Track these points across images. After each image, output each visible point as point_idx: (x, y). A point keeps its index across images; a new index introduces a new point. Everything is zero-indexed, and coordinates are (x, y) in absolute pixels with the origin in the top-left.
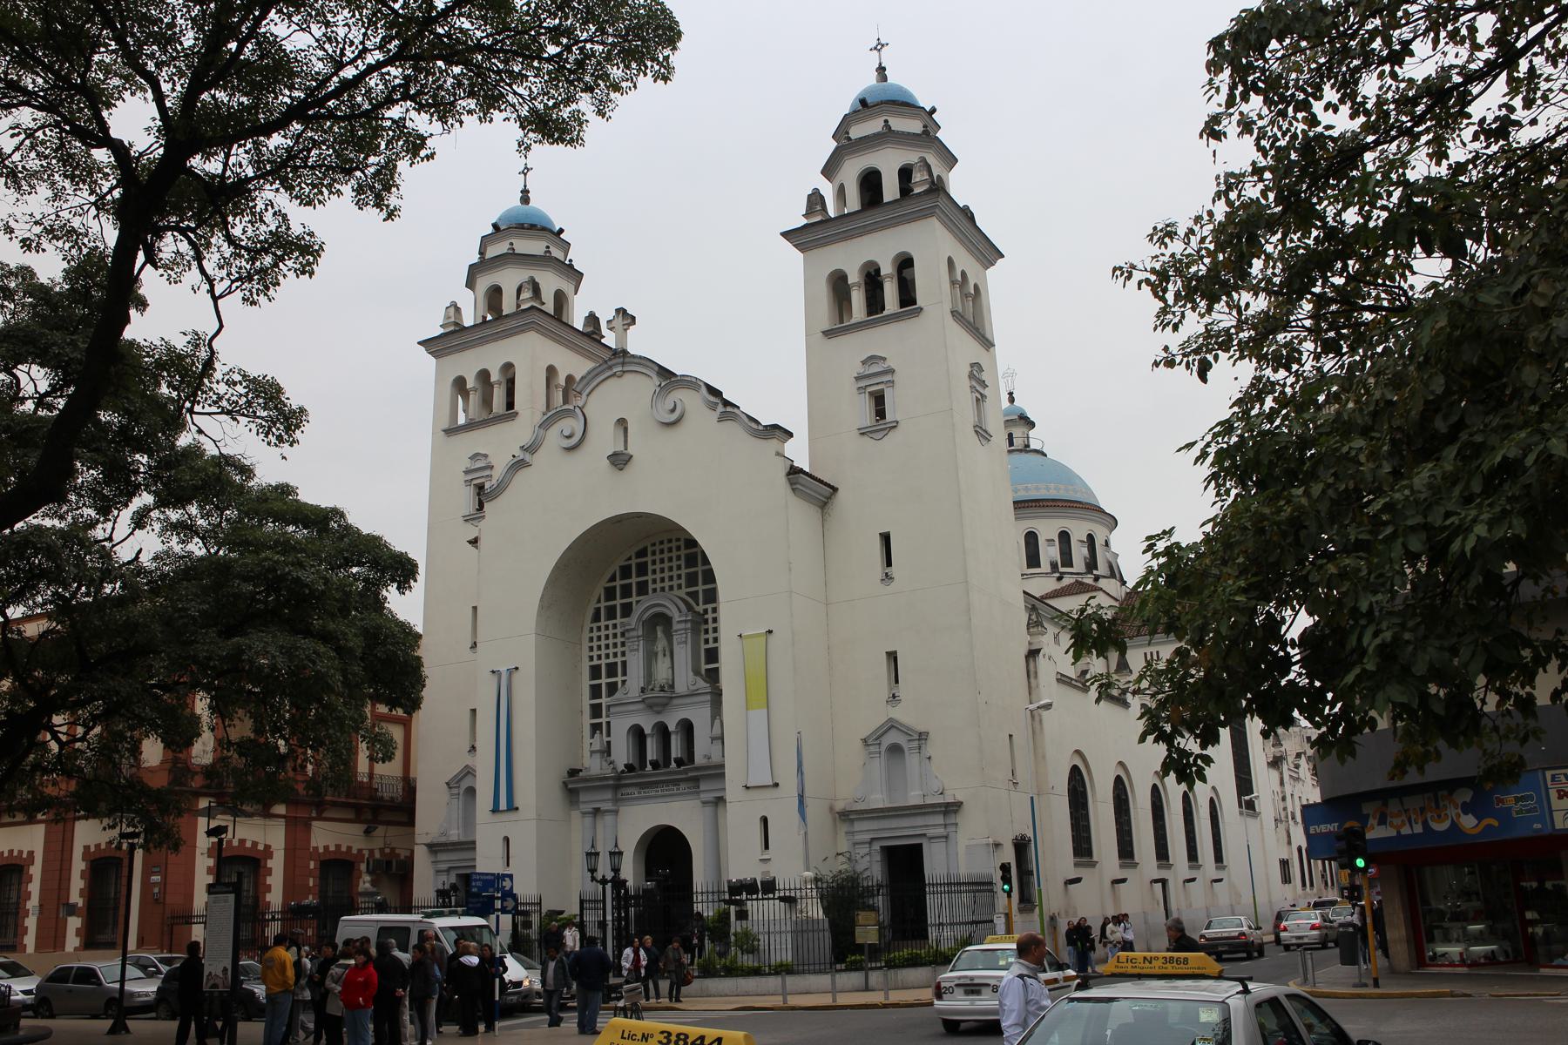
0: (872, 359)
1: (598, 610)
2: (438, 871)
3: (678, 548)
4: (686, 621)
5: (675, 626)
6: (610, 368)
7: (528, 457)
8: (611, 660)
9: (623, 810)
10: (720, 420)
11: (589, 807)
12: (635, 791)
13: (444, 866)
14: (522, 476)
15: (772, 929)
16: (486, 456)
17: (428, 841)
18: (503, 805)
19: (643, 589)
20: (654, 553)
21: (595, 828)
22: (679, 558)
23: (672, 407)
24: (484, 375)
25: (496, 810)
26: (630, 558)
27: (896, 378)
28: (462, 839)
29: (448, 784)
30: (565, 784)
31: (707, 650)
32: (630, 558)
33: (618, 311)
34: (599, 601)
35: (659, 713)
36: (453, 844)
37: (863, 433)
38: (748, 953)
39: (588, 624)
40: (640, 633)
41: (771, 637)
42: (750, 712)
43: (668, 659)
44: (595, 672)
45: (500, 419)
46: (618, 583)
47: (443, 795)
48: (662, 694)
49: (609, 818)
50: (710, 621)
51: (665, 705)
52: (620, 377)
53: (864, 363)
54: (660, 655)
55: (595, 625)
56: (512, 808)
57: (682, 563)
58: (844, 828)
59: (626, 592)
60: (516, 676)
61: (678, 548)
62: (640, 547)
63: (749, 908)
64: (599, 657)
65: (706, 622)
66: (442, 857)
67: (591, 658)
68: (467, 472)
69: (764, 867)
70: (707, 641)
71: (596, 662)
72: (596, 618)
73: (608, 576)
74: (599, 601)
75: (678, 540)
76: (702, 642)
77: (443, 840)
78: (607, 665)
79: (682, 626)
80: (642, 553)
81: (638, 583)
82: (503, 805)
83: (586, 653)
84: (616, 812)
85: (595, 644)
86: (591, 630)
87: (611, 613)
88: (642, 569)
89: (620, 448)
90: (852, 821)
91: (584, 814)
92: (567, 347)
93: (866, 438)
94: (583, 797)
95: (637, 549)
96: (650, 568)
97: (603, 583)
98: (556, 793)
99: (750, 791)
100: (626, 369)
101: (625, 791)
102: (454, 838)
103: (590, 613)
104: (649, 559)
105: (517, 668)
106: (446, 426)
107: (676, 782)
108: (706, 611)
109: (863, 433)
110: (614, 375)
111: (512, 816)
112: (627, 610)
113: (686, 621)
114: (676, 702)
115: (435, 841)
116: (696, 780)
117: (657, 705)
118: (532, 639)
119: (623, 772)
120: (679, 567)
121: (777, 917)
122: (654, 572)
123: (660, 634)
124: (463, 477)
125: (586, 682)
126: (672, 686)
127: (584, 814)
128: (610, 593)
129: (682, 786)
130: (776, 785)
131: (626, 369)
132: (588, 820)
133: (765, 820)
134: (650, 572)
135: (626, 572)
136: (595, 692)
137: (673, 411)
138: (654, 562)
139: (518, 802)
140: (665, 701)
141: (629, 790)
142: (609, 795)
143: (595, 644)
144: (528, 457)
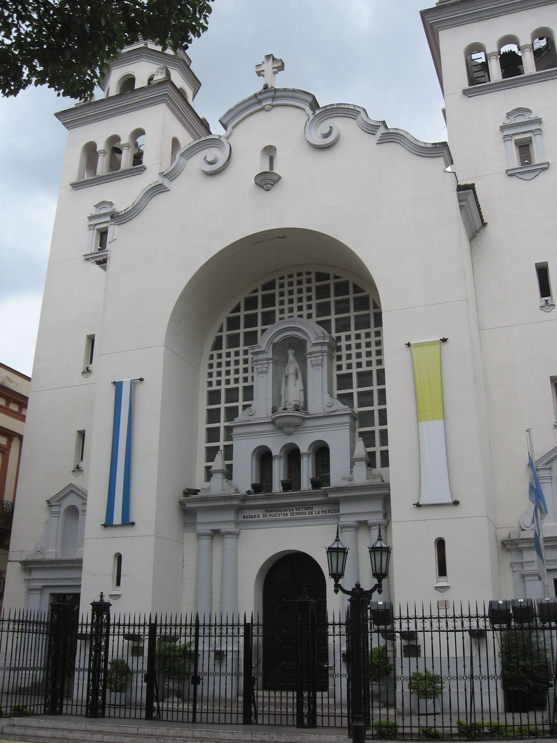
0: (520, 111)
1: (219, 340)
2: (30, 590)
3: (309, 281)
4: (322, 344)
5: (309, 349)
6: (260, 102)
7: (166, 182)
8: (232, 385)
9: (244, 533)
10: (380, 142)
11: (207, 529)
12: (260, 513)
13: (39, 585)
14: (160, 200)
15: (476, 673)
16: (111, 204)
17: (24, 559)
18: (117, 519)
19: (269, 319)
20: (282, 286)
21: (211, 551)
22: (309, 290)
23: (327, 130)
24: (115, 139)
25: (108, 524)
26: (256, 291)
27: (543, 127)
28: (59, 557)
29: (48, 502)
30: (182, 504)
31: (339, 377)
32: (256, 291)
33: (268, 57)
34: (221, 330)
35: (289, 434)
36: (51, 562)
37: (511, 174)
38: (116, 691)
39: (208, 351)
40: (270, 355)
41: (445, 346)
42: (423, 424)
43: (300, 383)
44: (214, 397)
45: (128, 173)
46: (242, 313)
47: (43, 513)
48: (297, 413)
49: (229, 541)
50: (344, 348)
51: (297, 426)
52: (268, 110)
53: (509, 115)
54: (292, 378)
55: (215, 353)
56: (127, 522)
57: (313, 294)
58: (509, 558)
59: (251, 321)
60: (141, 389)
61: (309, 281)
62: (268, 279)
63: (420, 642)
64: (219, 383)
65: (339, 349)
66: (36, 575)
67: (210, 384)
68: (91, 218)
69: (441, 597)
70: (339, 367)
71: (214, 387)
72: (217, 345)
73: (233, 306)
74: (221, 330)
75: (308, 273)
76: (335, 368)
77: (39, 557)
78: (227, 390)
79: (318, 348)
80: (270, 285)
81: (264, 314)
82: (117, 519)
83: (204, 379)
84: (237, 535)
85: (215, 370)
86: (212, 357)
87: (233, 341)
88: (269, 301)
89: (267, 169)
90: (521, 550)
91: (200, 536)
92: (188, 130)
93: (514, 180)
94: (200, 518)
95: (263, 282)
96: (278, 299)
97: (227, 313)
98: (173, 513)
99: (421, 509)
100: (275, 103)
101: (247, 513)
102: (52, 557)
103: (210, 341)
104: (277, 291)
105: (142, 380)
106: (74, 179)
107: (308, 506)
108: (339, 339)
109: (511, 174)
110: (263, 109)
111: (127, 531)
112: (251, 339)
113: (322, 344)
114: (309, 423)
115: (30, 559)
116: (336, 503)
117: (288, 425)
118: (161, 350)
119: (248, 492)
120: (309, 298)
121: (452, 654)
122: (282, 303)
123: (291, 357)
124: (86, 222)
125: (203, 406)
126: (305, 408)
127: (200, 536)
128: (233, 323)
129: (316, 509)
130: (456, 503)
131: (275, 103)
132: (205, 542)
133: (440, 544)
134: (277, 303)
135: (251, 303)
136: (213, 416)
137: (326, 136)
138: (282, 294)
139: (134, 516)
140: (298, 421)
141: (253, 513)
142: (231, 516)
143: (215, 370)
144: (166, 182)
